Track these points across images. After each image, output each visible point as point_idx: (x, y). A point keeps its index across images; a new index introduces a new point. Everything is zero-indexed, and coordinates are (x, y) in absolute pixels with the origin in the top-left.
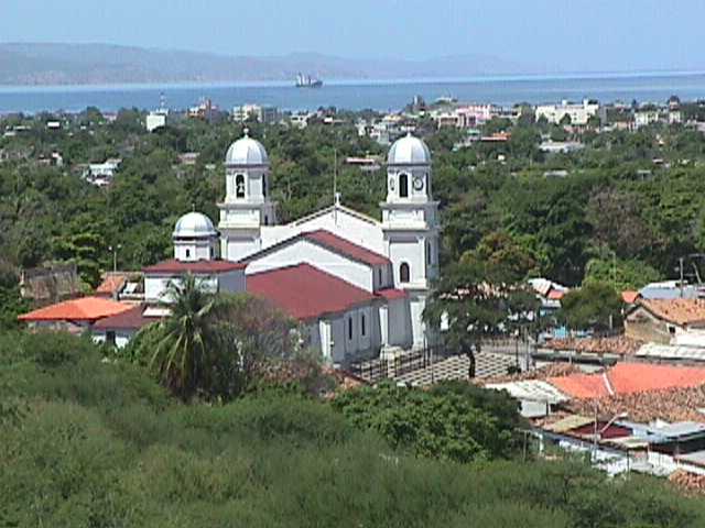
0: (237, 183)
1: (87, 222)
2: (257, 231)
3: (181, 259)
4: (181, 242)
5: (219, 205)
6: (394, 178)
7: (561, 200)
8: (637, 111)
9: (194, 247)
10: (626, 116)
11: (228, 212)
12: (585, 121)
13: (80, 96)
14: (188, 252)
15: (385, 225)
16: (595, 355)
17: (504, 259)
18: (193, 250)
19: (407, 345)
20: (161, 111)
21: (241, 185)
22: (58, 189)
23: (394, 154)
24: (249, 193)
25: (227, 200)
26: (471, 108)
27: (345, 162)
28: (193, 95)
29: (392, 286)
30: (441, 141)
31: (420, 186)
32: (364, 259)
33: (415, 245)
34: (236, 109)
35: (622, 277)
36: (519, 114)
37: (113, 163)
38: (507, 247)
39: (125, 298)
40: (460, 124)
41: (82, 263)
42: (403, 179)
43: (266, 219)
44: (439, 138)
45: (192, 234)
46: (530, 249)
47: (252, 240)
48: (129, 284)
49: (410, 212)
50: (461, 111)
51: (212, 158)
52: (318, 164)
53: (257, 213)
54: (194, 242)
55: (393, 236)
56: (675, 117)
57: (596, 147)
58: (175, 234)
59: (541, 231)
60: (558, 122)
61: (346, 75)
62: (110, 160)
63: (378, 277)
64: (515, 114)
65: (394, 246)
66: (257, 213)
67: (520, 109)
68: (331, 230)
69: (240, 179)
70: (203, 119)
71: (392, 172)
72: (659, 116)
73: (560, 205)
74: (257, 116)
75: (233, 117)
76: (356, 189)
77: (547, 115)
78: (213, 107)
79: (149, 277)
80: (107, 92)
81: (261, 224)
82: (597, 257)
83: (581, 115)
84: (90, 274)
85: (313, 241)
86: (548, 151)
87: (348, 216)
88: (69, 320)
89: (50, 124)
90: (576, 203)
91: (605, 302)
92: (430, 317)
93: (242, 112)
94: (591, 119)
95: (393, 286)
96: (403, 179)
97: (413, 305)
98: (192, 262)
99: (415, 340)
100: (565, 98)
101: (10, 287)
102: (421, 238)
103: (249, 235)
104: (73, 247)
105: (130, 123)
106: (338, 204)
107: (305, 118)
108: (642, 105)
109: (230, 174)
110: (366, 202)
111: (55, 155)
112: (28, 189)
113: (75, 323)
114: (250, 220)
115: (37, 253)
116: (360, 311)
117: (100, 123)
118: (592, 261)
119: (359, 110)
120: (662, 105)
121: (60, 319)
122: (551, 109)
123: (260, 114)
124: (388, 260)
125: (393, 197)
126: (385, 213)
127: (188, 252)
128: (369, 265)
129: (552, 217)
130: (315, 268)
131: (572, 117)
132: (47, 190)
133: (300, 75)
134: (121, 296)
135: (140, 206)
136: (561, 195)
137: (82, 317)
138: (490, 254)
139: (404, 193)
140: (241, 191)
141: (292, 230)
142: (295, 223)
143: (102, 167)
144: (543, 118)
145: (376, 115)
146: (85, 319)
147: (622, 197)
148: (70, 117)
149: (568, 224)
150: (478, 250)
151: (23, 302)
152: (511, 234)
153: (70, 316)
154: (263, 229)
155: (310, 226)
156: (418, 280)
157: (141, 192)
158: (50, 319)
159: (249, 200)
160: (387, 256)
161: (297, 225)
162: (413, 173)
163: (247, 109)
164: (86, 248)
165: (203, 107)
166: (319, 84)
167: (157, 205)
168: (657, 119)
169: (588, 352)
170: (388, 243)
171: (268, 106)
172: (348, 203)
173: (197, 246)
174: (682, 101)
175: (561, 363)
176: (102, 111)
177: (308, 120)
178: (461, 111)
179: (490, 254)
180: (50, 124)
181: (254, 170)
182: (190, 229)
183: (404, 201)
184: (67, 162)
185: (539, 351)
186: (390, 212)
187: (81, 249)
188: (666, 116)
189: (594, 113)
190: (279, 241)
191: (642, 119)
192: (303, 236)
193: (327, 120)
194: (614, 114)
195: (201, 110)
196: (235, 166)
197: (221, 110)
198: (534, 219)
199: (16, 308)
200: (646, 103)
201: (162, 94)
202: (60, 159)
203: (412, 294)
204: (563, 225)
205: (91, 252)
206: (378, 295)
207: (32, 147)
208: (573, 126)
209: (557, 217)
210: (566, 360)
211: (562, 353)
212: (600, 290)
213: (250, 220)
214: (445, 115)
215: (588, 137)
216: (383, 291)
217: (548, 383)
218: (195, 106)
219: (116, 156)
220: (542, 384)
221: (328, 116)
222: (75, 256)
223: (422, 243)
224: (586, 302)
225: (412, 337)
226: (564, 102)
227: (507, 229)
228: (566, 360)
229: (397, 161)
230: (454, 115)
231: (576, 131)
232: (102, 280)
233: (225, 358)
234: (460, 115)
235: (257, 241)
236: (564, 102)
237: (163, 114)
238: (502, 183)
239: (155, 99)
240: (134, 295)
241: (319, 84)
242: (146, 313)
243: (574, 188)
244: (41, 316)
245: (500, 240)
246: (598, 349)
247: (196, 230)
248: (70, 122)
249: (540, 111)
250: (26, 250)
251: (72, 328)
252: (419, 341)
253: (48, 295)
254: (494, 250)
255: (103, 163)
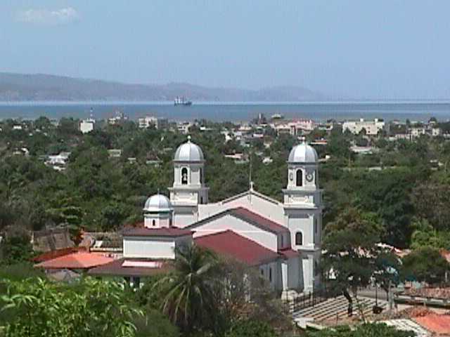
0: (183, 174)
1: (63, 198)
2: (195, 207)
3: (149, 227)
4: (149, 215)
5: (169, 188)
6: (293, 173)
7: (393, 189)
8: (410, 127)
9: (158, 219)
10: (404, 130)
11: (175, 194)
12: (376, 133)
13: (36, 108)
14: (154, 222)
15: (286, 204)
16: (441, 301)
17: (356, 230)
18: (157, 221)
19: (300, 289)
20: (91, 120)
21: (185, 175)
22: (35, 173)
23: (294, 154)
24: (190, 182)
25: (174, 186)
26: (299, 122)
27: (224, 158)
28: (111, 110)
29: (289, 248)
30: (284, 144)
31: (310, 179)
32: (271, 228)
33: (306, 219)
34: (140, 120)
35: (438, 243)
36: (332, 127)
37: (65, 155)
38: (357, 220)
39: (94, 251)
40: (291, 132)
41: (69, 226)
42: (299, 173)
43: (202, 199)
44: (334, 145)
45: (158, 210)
46: (374, 223)
47: (191, 213)
48: (97, 242)
49: (302, 194)
50: (292, 124)
51: (132, 153)
52: (241, 163)
53: (196, 195)
54: (158, 215)
55: (292, 213)
56: (436, 132)
57: (388, 150)
58: (145, 209)
59: (380, 209)
60: (357, 132)
61: (207, 98)
62: (62, 153)
63: (280, 242)
64: (328, 127)
65: (291, 220)
66: (196, 195)
67: (331, 123)
68: (247, 208)
69: (184, 171)
70: (118, 126)
71: (291, 168)
72: (426, 131)
73: (393, 193)
74: (155, 125)
75: (138, 125)
76: (240, 177)
77: (351, 129)
78: (126, 118)
79: (127, 239)
80: (53, 106)
81: (198, 203)
82: (418, 228)
83: (374, 128)
84: (75, 235)
85: (236, 216)
86: (357, 153)
87: (270, 203)
88: (70, 269)
89: (15, 127)
90: (405, 191)
91: (435, 261)
92: (319, 270)
93: (144, 121)
94: (380, 132)
95: (291, 248)
96: (299, 173)
97: (304, 261)
98: (157, 229)
99: (305, 287)
100: (362, 118)
101: (25, 244)
102: (311, 215)
103: (190, 210)
104: (62, 215)
105: (69, 128)
106: (252, 190)
107: (187, 127)
108: (413, 122)
109: (177, 167)
110: (275, 191)
111: (24, 149)
112: (14, 172)
113: (73, 271)
114: (192, 200)
115: (43, 219)
116: (269, 265)
117: (49, 127)
118: (416, 232)
119: (222, 122)
120: (427, 123)
121: (64, 268)
122: (353, 124)
123: (156, 123)
124: (288, 229)
125: (292, 185)
126: (286, 197)
127: (154, 222)
128: (274, 232)
129: (388, 201)
130: (237, 234)
131: (367, 130)
132: (27, 173)
133: (178, 98)
134: (92, 249)
135: (96, 186)
136: (393, 186)
137: (79, 267)
138: (346, 225)
139: (299, 183)
140: (185, 179)
141: (219, 207)
142: (221, 203)
143: (59, 157)
144: (348, 131)
145: (234, 126)
146: (81, 268)
147: (437, 188)
148: (28, 123)
149: (398, 206)
150: (338, 222)
151: (35, 255)
152: (359, 211)
153: (71, 266)
154: (199, 205)
155: (233, 204)
156: (308, 244)
157: (95, 177)
158: (57, 268)
159: (306, 188)
160: (287, 226)
161: (223, 203)
162: (306, 169)
163: (148, 120)
164: (72, 217)
165: (118, 118)
166: (189, 104)
167: (108, 186)
168: (424, 132)
169: (436, 299)
170: (287, 217)
171: (162, 118)
172: (261, 188)
173: (160, 218)
174: (438, 120)
175: (419, 307)
176: (50, 120)
177: (189, 129)
178: (292, 124)
179: (346, 225)
180: (15, 127)
181: (309, 166)
182: (156, 206)
183: (299, 188)
184: (33, 154)
185: (400, 297)
186: (290, 196)
187: (69, 217)
188: (430, 131)
189: (381, 128)
190: (211, 216)
191: (415, 132)
192: (228, 212)
193: (202, 129)
194: (395, 130)
195: (116, 121)
196: (296, 163)
197: (130, 120)
198: (374, 201)
199: (30, 259)
200: (416, 122)
201: (92, 109)
202: (27, 152)
203: (304, 254)
204: (396, 206)
205: (75, 219)
206: (281, 254)
207: (8, 143)
208: (369, 135)
209: (391, 200)
210: (422, 304)
211: (416, 298)
212: (430, 253)
213: (192, 200)
214: (281, 127)
215: (381, 144)
216: (284, 252)
217: (414, 322)
218: (112, 118)
219: (65, 150)
220: (409, 322)
221: (202, 126)
222: (64, 222)
223: (311, 218)
224: (420, 261)
225: (303, 284)
226: (362, 120)
227: (356, 208)
228: (422, 304)
229: (295, 161)
230: (287, 127)
231: (372, 140)
232: (82, 239)
233: (212, 308)
234: (292, 127)
235: (196, 214)
236: (362, 120)
237: (92, 122)
238: (341, 175)
239: (86, 113)
240: (101, 249)
241: (189, 104)
242: (124, 265)
243: (403, 181)
244: (50, 265)
245: (352, 215)
246: (442, 297)
247: (160, 207)
248: (28, 126)
249: (345, 126)
250: (36, 218)
251: (72, 274)
252: (308, 287)
253: (49, 250)
254: (348, 223)
255: (58, 154)
